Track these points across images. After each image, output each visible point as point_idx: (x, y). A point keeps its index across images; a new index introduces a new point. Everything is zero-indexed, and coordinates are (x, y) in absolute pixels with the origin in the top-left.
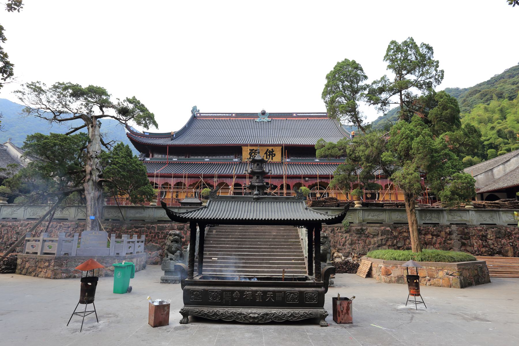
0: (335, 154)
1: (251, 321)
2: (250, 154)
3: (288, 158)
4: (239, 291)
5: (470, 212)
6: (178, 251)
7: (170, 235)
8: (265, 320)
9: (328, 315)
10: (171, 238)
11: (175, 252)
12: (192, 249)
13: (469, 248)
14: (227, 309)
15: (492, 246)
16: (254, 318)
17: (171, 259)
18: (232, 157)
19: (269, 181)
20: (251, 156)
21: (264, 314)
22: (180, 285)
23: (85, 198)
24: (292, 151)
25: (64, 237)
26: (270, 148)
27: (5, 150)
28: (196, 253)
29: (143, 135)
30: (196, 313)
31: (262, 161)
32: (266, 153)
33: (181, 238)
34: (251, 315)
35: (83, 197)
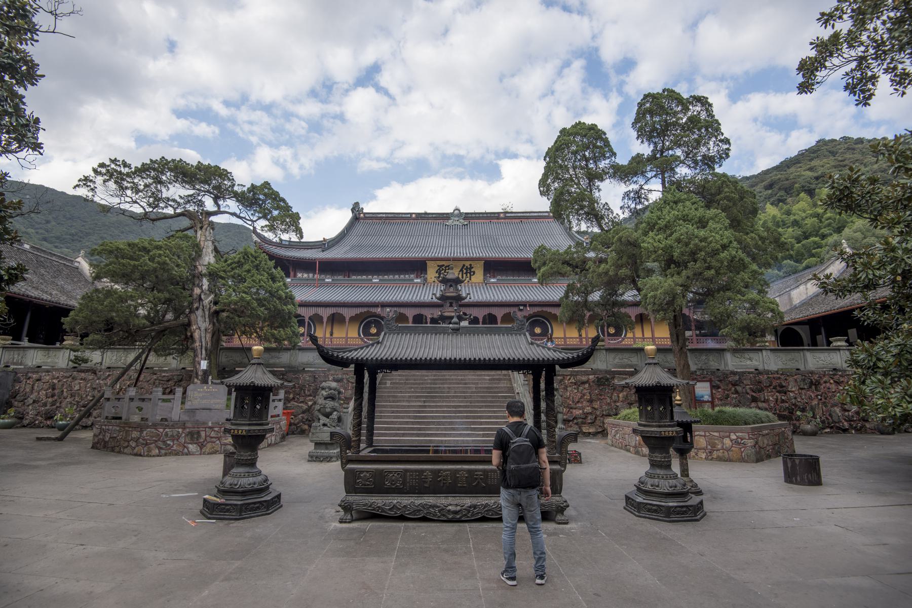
0: (572, 264)
1: (450, 517)
2: (439, 272)
3: (494, 277)
4: (416, 471)
5: (764, 352)
6: (335, 413)
7: (323, 389)
8: (472, 516)
9: (568, 506)
10: (324, 393)
11: (331, 414)
12: (358, 409)
13: (760, 404)
14: (412, 500)
15: (793, 401)
16: (456, 512)
17: (324, 425)
18: (412, 276)
19: (468, 311)
20: (440, 274)
21: (470, 507)
22: (339, 462)
23: (192, 336)
24: (496, 267)
25: (160, 393)
26: (467, 264)
27: (77, 268)
28: (364, 413)
29: (281, 244)
30: (364, 505)
31: (458, 281)
32: (462, 270)
33: (339, 393)
34: (450, 507)
35: (189, 334)
